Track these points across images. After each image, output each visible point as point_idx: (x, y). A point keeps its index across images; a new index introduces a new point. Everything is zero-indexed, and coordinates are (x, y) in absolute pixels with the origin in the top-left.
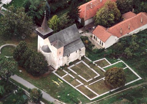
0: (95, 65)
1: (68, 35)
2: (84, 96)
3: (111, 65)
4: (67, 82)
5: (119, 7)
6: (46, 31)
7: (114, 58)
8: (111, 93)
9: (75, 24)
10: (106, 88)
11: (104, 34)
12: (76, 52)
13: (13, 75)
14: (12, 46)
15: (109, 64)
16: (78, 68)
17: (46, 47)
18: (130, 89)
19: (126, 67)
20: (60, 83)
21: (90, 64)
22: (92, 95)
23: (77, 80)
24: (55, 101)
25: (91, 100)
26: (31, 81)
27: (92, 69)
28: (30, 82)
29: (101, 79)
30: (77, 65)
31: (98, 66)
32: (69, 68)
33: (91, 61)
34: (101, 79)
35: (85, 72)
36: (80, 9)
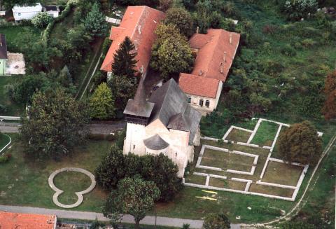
0: (229, 143)
1: (175, 102)
2: (274, 199)
3: (255, 131)
4: (225, 189)
5: (153, 58)
6: (148, 108)
7: (247, 120)
8: (307, 175)
9: (172, 79)
10: (289, 171)
11: (203, 84)
12: (134, 146)
13: (227, 219)
14: (64, 172)
15: (251, 134)
16: (211, 160)
17: (157, 139)
18: (325, 157)
19: (278, 126)
20: (213, 196)
21: (221, 144)
22: (288, 193)
23: (233, 179)
24: (241, 227)
25: (293, 199)
26: (166, 214)
27: (234, 152)
28: (167, 216)
29: (267, 162)
30: (204, 155)
31: (238, 143)
32: (198, 165)
33: (217, 140)
34: (267, 162)
35: (230, 162)
36: (135, 62)
